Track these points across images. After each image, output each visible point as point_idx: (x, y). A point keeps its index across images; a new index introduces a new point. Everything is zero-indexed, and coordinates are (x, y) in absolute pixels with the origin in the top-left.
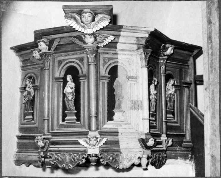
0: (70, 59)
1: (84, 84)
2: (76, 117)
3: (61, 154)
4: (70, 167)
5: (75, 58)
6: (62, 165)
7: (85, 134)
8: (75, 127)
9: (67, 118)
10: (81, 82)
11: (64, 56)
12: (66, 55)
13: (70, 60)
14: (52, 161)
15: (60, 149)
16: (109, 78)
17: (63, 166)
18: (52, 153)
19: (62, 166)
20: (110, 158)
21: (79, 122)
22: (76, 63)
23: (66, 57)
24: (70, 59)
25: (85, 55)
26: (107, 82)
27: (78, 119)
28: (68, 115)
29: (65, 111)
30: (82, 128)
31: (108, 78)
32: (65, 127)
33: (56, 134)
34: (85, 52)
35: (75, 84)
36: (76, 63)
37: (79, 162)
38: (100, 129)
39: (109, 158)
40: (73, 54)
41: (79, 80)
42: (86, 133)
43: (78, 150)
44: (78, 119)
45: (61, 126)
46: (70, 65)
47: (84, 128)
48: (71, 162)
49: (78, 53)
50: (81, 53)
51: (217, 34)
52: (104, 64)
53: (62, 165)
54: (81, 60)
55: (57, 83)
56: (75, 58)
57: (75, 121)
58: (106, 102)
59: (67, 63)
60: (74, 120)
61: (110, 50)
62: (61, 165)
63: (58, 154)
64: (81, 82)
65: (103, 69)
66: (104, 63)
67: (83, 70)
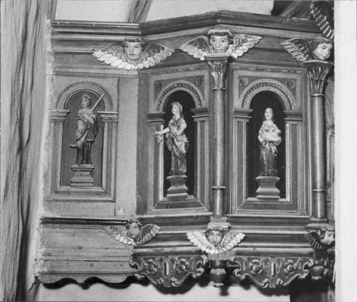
0: (265, 78)
1: (202, 128)
2: (187, 187)
3: (154, 259)
4: (173, 284)
5: (277, 79)
6: (158, 280)
7: (205, 221)
8: (277, 209)
9: (259, 190)
10: (196, 122)
11: (253, 70)
12: (257, 70)
13: (268, 81)
14: (139, 273)
15: (258, 249)
16: (250, 114)
17: (160, 281)
18: (241, 257)
19: (158, 282)
20: (252, 267)
21: (192, 197)
22: (263, 85)
23: (259, 74)
24: (265, 78)
25: (205, 73)
26: (247, 123)
27: (191, 191)
28: (172, 184)
29: (257, 176)
30: (293, 211)
31: (249, 115)
32: (256, 207)
33: (241, 220)
34: (179, 70)
35: (187, 127)
36: (189, 87)
37: (296, 275)
38: (232, 213)
39: (250, 268)
40: (273, 71)
41: (193, 118)
42: (303, 221)
43: (297, 252)
44: (191, 191)
45: (161, 206)
46: (267, 90)
47: (296, 211)
48: (177, 275)
49: (191, 69)
50: (289, 71)
51: (273, 46)
52: (241, 89)
53: (158, 280)
54: (200, 79)
55: (239, 120)
56: (277, 79)
57: (279, 197)
58: (199, 159)
59: (258, 86)
60: (275, 195)
61: (90, 68)
62: (156, 281)
63: (149, 260)
64: (196, 122)
65: (296, 98)
66: (241, 85)
67: (202, 100)
